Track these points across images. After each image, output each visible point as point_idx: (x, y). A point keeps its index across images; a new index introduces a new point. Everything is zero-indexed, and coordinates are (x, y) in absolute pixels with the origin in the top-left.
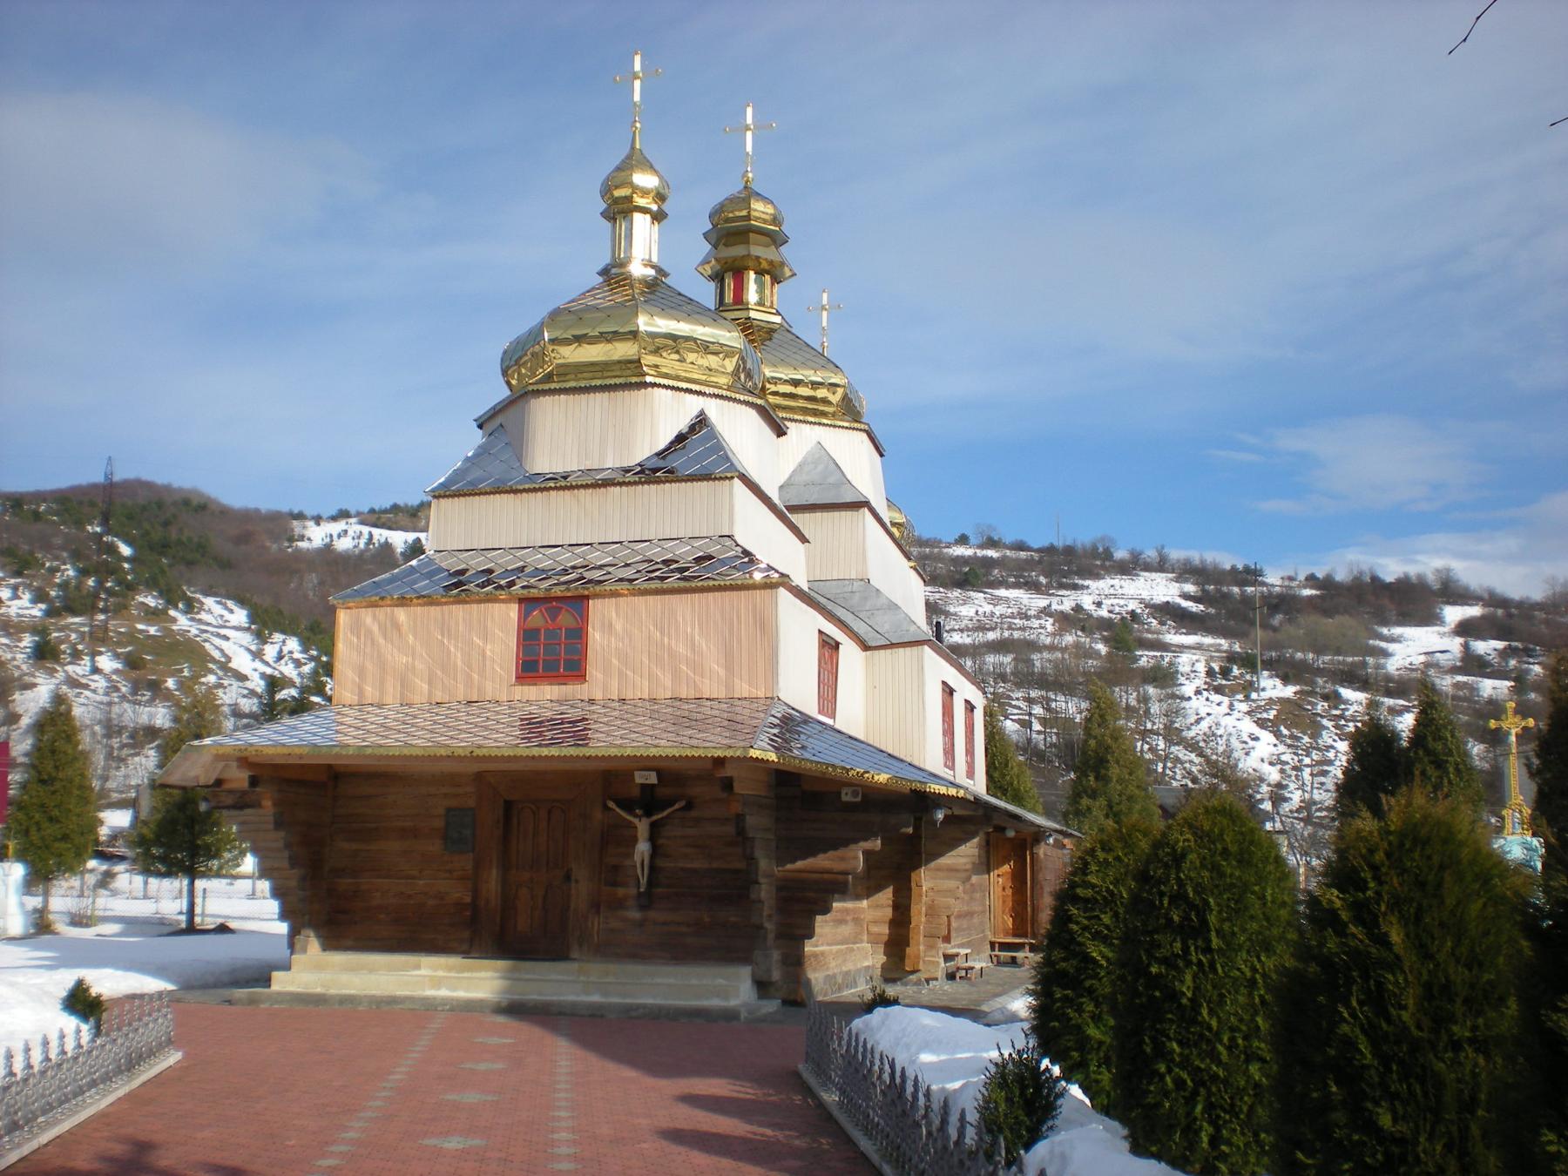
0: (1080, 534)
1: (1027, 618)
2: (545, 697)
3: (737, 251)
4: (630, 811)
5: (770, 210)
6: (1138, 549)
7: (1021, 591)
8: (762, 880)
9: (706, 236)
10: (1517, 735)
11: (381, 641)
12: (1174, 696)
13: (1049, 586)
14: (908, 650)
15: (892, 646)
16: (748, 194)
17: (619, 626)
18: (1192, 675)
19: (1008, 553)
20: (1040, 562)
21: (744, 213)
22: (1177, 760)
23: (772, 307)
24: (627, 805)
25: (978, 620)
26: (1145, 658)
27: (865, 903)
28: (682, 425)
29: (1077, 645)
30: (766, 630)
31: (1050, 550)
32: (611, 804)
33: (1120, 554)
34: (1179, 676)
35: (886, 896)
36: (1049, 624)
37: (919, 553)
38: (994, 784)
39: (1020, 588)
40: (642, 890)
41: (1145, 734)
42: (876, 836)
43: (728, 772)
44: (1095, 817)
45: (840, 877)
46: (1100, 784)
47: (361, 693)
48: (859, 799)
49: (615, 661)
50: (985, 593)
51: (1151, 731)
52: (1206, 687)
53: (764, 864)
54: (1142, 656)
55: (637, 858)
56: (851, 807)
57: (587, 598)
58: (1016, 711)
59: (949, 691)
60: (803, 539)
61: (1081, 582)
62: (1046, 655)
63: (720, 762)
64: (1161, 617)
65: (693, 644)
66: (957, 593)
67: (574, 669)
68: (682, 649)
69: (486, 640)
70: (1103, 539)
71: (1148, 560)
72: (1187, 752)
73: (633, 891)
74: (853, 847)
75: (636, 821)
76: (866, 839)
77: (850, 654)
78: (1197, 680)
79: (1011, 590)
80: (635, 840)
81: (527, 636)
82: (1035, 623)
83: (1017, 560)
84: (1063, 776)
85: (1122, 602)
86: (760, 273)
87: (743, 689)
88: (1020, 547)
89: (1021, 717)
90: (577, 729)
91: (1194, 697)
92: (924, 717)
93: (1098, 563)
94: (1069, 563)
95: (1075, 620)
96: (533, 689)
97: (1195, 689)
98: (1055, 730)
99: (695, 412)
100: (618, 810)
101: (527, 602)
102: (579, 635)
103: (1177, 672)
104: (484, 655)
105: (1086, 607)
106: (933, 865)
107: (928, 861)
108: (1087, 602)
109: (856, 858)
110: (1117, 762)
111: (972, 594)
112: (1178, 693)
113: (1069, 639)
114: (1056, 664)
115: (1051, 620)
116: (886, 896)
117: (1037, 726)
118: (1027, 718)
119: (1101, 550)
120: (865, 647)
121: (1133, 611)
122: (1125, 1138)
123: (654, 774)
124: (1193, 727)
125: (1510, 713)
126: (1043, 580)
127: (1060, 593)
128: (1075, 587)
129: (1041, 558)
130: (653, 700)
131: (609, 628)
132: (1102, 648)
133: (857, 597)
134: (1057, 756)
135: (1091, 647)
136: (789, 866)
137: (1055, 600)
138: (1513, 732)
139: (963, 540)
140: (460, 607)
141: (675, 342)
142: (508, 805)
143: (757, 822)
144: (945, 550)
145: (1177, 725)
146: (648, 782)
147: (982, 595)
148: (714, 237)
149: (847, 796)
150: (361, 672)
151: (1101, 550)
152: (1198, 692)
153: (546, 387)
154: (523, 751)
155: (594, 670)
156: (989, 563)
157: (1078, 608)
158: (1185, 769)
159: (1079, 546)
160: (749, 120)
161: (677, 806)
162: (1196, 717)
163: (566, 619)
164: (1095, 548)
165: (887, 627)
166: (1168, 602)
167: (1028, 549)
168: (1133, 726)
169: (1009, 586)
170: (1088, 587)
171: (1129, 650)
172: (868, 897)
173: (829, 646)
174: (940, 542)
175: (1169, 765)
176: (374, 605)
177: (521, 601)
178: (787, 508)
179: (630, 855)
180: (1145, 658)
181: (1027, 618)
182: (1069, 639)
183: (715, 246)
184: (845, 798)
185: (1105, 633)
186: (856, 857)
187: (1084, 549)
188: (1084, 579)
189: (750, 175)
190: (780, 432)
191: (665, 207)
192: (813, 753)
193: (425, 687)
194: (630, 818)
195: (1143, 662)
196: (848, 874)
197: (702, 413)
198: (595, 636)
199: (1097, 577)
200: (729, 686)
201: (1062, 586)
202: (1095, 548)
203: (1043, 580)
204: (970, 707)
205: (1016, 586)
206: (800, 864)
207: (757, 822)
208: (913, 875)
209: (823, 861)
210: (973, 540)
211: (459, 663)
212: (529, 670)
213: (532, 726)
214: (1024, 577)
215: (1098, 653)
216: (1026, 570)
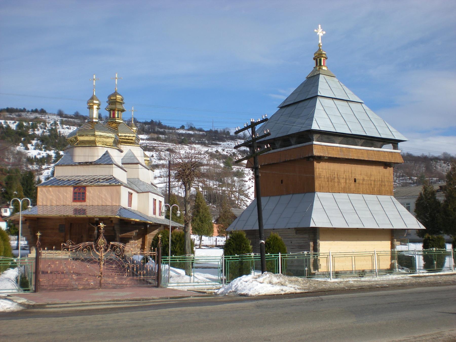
0: (219, 128)
1: (201, 154)
2: (78, 204)
3: (113, 107)
4: (94, 225)
5: (121, 97)
7: (200, 145)
8: (117, 237)
9: (107, 102)
11: (47, 194)
12: (243, 181)
13: (209, 144)
14: (146, 193)
15: (143, 192)
16: (115, 94)
17: (92, 192)
18: (249, 174)
19: (196, 132)
20: (206, 135)
21: (115, 98)
22: (242, 200)
23: (121, 118)
24: (93, 224)
25: (185, 155)
27: (137, 241)
28: (104, 153)
29: (215, 164)
30: (119, 194)
31: (210, 131)
32: (90, 224)
33: (232, 133)
34: (245, 174)
35: (141, 240)
36: (207, 156)
37: (168, 132)
39: (199, 144)
40: (272, 233)
41: (232, 192)
42: (137, 230)
43: (112, 219)
44: (197, 221)
45: (131, 237)
46: (198, 213)
47: (43, 203)
48: (134, 223)
49: (91, 199)
50: (188, 146)
51: (235, 191)
52: (252, 178)
53: (117, 234)
54: (234, 168)
55: (95, 233)
56: (133, 224)
57: (86, 187)
58: (194, 185)
59: (155, 200)
60: (126, 171)
61: (218, 143)
62: (205, 167)
63: (110, 218)
64: (242, 155)
65: (105, 195)
66: (180, 145)
67: (84, 200)
68: (103, 196)
69: (67, 194)
71: (240, 136)
72: (245, 198)
73: (94, 239)
74: (133, 231)
75: (94, 227)
76: (135, 230)
77: (135, 195)
78: (250, 176)
79: (196, 145)
80: (94, 230)
81: (75, 193)
82: (202, 156)
83: (199, 135)
84: (208, 204)
85: (231, 149)
86: (118, 111)
87: (114, 204)
88: (201, 130)
89: (195, 186)
90: (83, 211)
91: (248, 181)
93: (225, 136)
94: (215, 136)
96: (76, 203)
97: (249, 178)
98: (206, 191)
99: (106, 151)
100: (92, 225)
101: (75, 188)
102: (84, 193)
103: (244, 173)
104: (66, 197)
105: (219, 151)
106: (150, 234)
107: (148, 234)
108: (220, 150)
109: (134, 233)
110: (202, 208)
111: (184, 146)
112: (244, 180)
113: (212, 162)
114: (208, 170)
115: (208, 155)
116: (141, 240)
117: (201, 189)
118: (197, 187)
120: (138, 193)
121: (234, 152)
124: (247, 190)
126: (207, 142)
127: (212, 146)
128: (217, 144)
129: (207, 134)
130: (98, 206)
131: (90, 192)
132: (222, 165)
133: (136, 182)
134: (206, 199)
135: (219, 165)
136: (122, 235)
137: (210, 148)
139: (183, 127)
140: (62, 188)
141: (101, 136)
142: (71, 224)
143: (116, 227)
144: (177, 131)
145: (243, 189)
147: (187, 146)
148: (109, 102)
149: (132, 223)
150: (43, 199)
152: (250, 179)
153: (77, 146)
155: (87, 200)
156: (190, 135)
157: (217, 151)
158: (244, 203)
160: (117, 76)
162: (249, 187)
163: (82, 191)
164: (224, 131)
165: (142, 188)
166: (245, 150)
167: (203, 131)
168: (230, 189)
169: (196, 144)
170: (220, 144)
171: (230, 166)
172: (137, 240)
173: (130, 194)
174: (175, 128)
175: (239, 201)
176: (45, 187)
177: (73, 187)
179: (94, 233)
181: (201, 154)
182: (212, 162)
183: (109, 104)
185: (224, 160)
186: (134, 233)
187: (221, 132)
188: (220, 142)
189: (117, 89)
191: (100, 107)
192: (126, 216)
193: (55, 202)
194: (93, 226)
195: (234, 169)
196: (132, 236)
197: (107, 151)
198: (87, 194)
199: (224, 141)
200: (112, 203)
201: (212, 144)
202: (224, 131)
203: (207, 142)
205: (198, 143)
206: (124, 234)
207: (116, 227)
208: (146, 236)
209: (128, 234)
210: (186, 128)
211: (62, 198)
212: (75, 200)
213: (76, 211)
214: (200, 140)
215: (221, 167)
216: (201, 138)
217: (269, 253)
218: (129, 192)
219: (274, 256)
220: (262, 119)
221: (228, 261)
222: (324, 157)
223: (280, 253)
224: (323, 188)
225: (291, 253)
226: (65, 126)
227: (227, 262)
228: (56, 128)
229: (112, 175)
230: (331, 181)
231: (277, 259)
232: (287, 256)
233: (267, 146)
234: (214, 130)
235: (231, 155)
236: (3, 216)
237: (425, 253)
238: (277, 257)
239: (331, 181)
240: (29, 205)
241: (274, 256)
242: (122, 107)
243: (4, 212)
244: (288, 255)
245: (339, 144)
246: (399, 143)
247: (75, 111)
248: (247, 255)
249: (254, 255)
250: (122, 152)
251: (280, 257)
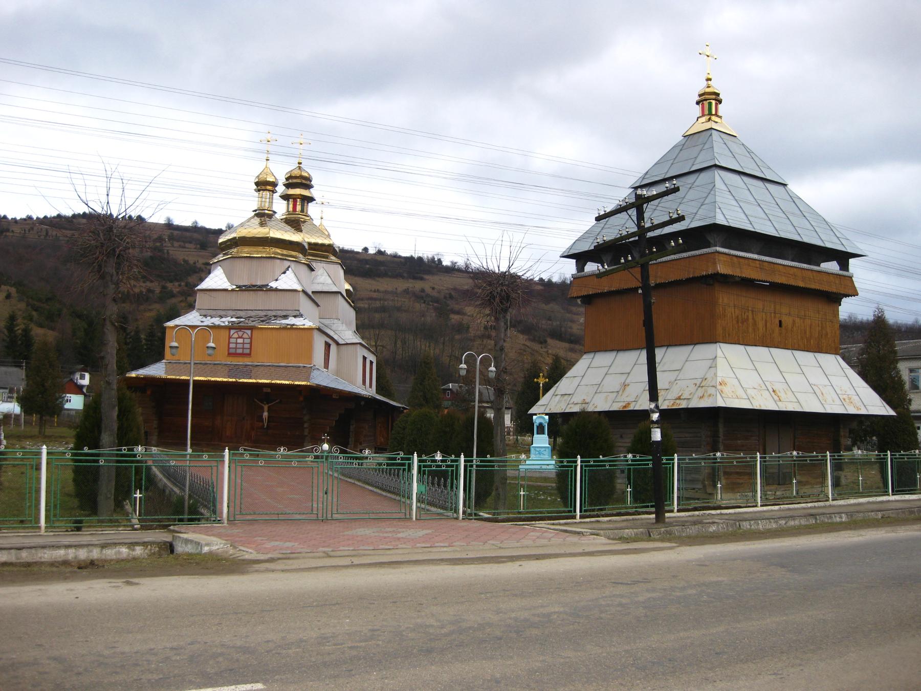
26: (455, 318)
38: (379, 390)
55: (264, 417)
59: (365, 358)
60: (318, 305)
75: (263, 405)
95: (421, 297)
119: (436, 259)
128: (422, 279)
151: (436, 259)
154: (164, 376)
157: (423, 291)
161: (277, 401)
173: (328, 346)
178: (313, 292)
180: (455, 318)
184: (334, 397)
190: (312, 270)
204: (371, 363)
217: (815, 453)
218: (325, 342)
219: (568, 462)
220: (666, 189)
221: (427, 469)
222: (732, 276)
223: (579, 457)
224: (729, 335)
225: (694, 455)
227: (585, 470)
229: (299, 310)
230: (742, 323)
231: (454, 468)
232: (748, 459)
234: (416, 257)
235: (445, 297)
237: (129, 450)
238: (574, 464)
239: (742, 323)
240: (210, 342)
241: (568, 462)
242: (310, 193)
244: (770, 457)
245: (759, 254)
246: (850, 260)
248: (710, 455)
249: (632, 458)
250: (314, 270)
251: (676, 461)
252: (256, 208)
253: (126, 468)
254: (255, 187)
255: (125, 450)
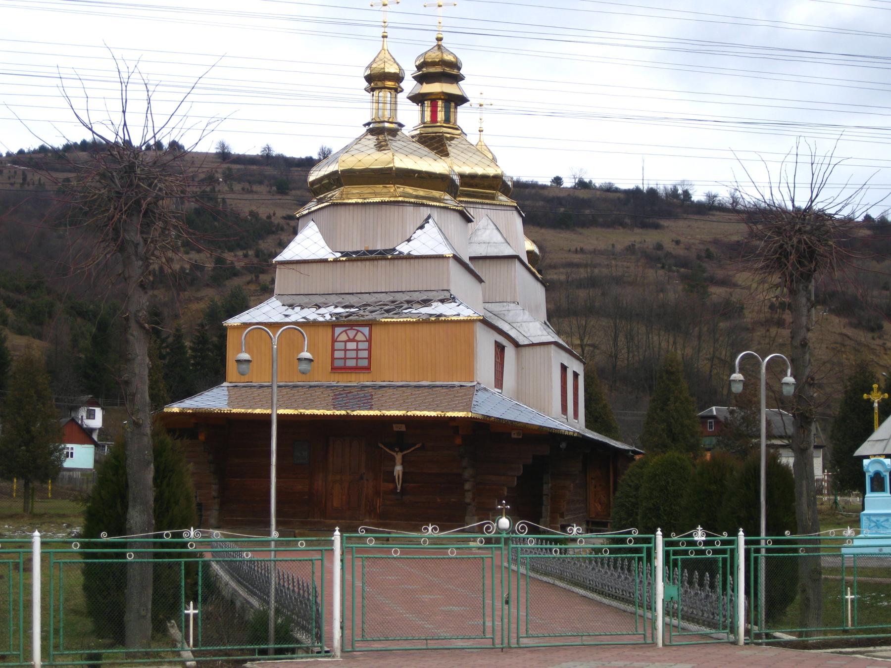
4: (392, 450)
6: (713, 193)
10: (878, 402)
26: (717, 293)
38: (591, 423)
55: (396, 474)
59: (564, 368)
60: (480, 281)
70: (683, 183)
75: (394, 454)
92: (552, 386)
119: (680, 191)
122: (558, 180)
123: (404, 426)
125: (875, 390)
128: (657, 227)
138: (876, 401)
146: (401, 430)
149: (514, 436)
157: (659, 247)
159: (662, 187)
161: (417, 447)
164: (675, 190)
173: (500, 349)
178: (471, 258)
180: (717, 293)
204: (576, 375)
218: (496, 342)
221: (679, 557)
226: (237, 187)
228: (213, 190)
231: (727, 556)
233: (85, 436)
236: (86, 428)
237: (174, 535)
240: (303, 351)
243: (87, 418)
247: (264, 145)
252: (369, 120)
253: (170, 566)
254: (365, 84)
255: (167, 535)
